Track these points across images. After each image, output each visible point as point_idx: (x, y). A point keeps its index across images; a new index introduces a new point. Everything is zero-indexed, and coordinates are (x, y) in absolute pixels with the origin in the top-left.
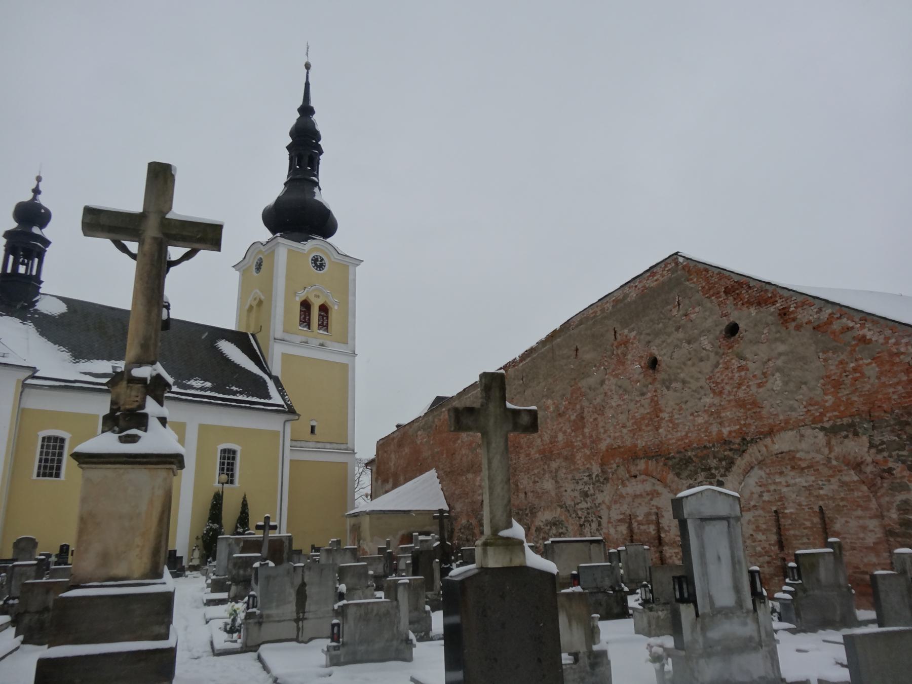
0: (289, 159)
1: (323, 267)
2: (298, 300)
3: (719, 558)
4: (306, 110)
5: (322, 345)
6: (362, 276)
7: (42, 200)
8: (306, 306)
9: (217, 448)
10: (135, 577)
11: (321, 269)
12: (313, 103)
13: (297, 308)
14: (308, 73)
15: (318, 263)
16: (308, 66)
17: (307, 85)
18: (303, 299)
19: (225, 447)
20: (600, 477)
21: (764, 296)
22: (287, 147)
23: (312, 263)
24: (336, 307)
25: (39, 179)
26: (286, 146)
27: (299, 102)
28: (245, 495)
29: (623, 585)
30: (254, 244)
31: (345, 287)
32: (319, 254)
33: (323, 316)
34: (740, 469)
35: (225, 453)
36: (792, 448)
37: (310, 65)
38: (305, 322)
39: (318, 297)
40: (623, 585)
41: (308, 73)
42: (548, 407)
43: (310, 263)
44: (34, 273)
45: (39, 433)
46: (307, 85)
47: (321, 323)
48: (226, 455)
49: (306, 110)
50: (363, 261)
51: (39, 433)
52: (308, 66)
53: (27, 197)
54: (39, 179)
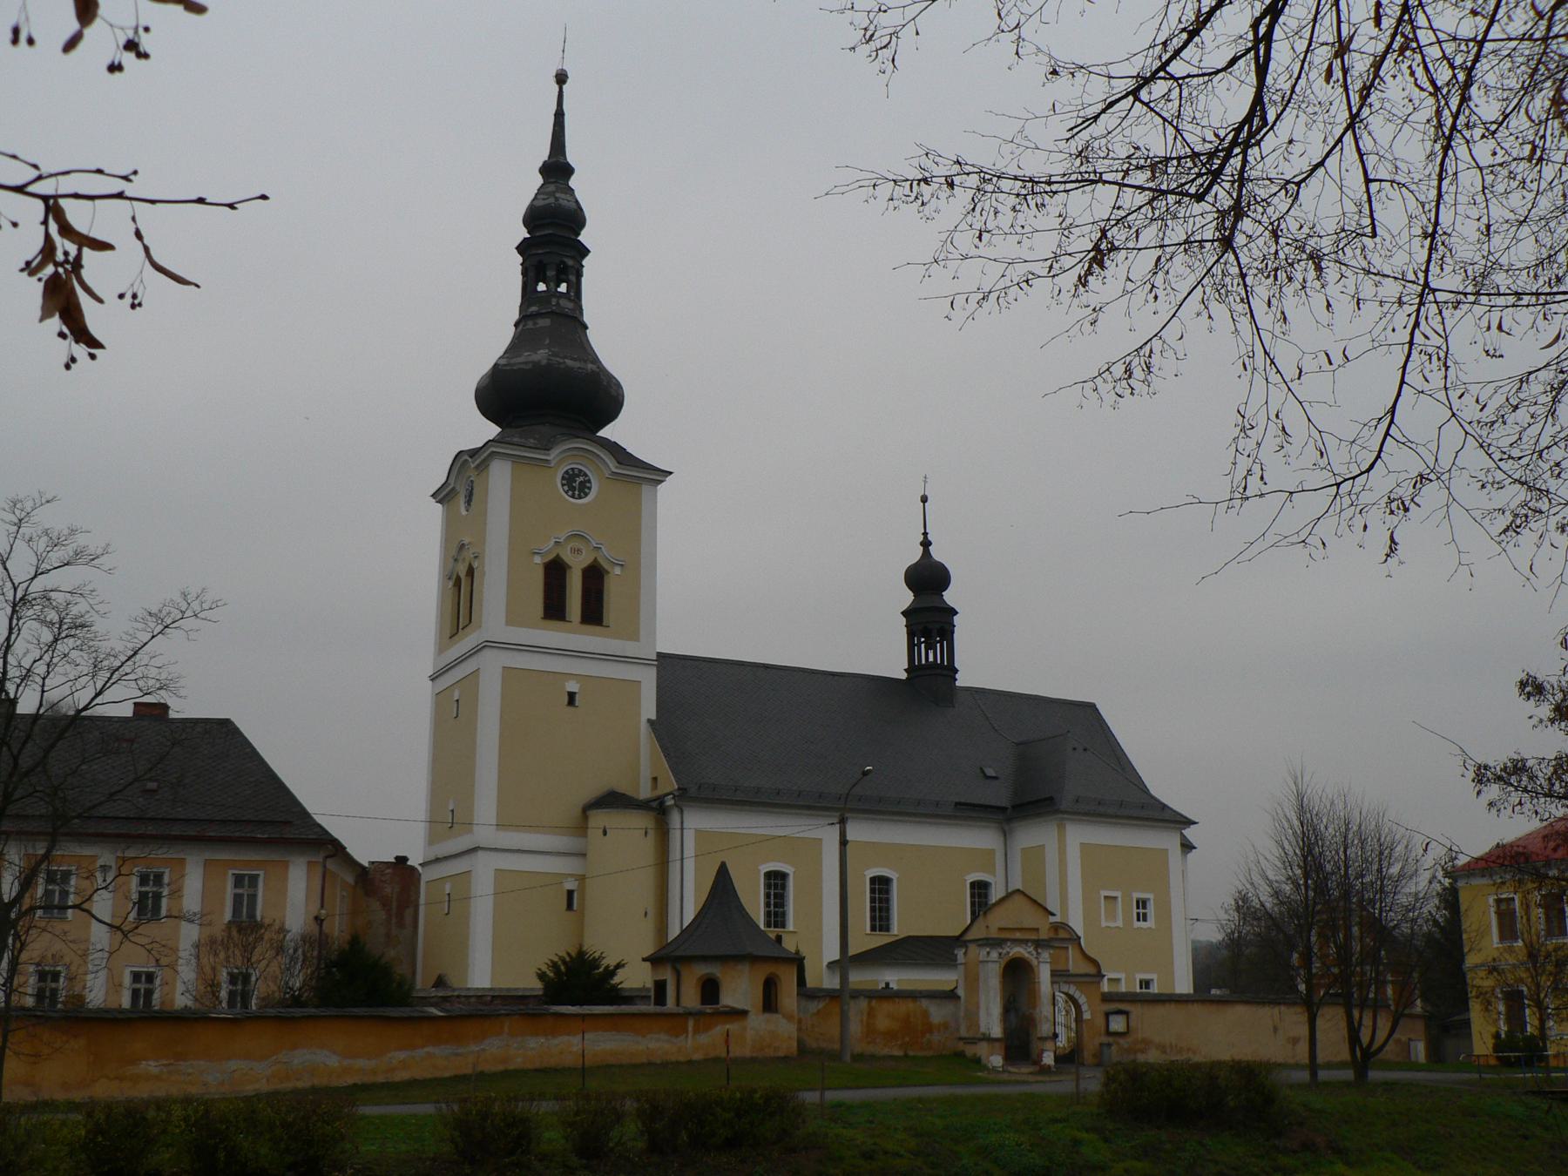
0: (522, 274)
1: (587, 490)
4: (557, 170)
8: (555, 572)
9: (759, 871)
11: (567, 476)
12: (572, 157)
16: (561, 78)
17: (559, 116)
19: (976, 879)
20: (153, 662)
22: (517, 248)
23: (563, 485)
26: (516, 244)
27: (543, 153)
28: (1195, 823)
30: (456, 456)
35: (770, 879)
36: (108, 864)
37: (567, 76)
39: (579, 551)
43: (559, 485)
45: (761, 868)
46: (559, 116)
48: (772, 881)
49: (557, 170)
50: (671, 473)
51: (761, 868)
52: (561, 78)
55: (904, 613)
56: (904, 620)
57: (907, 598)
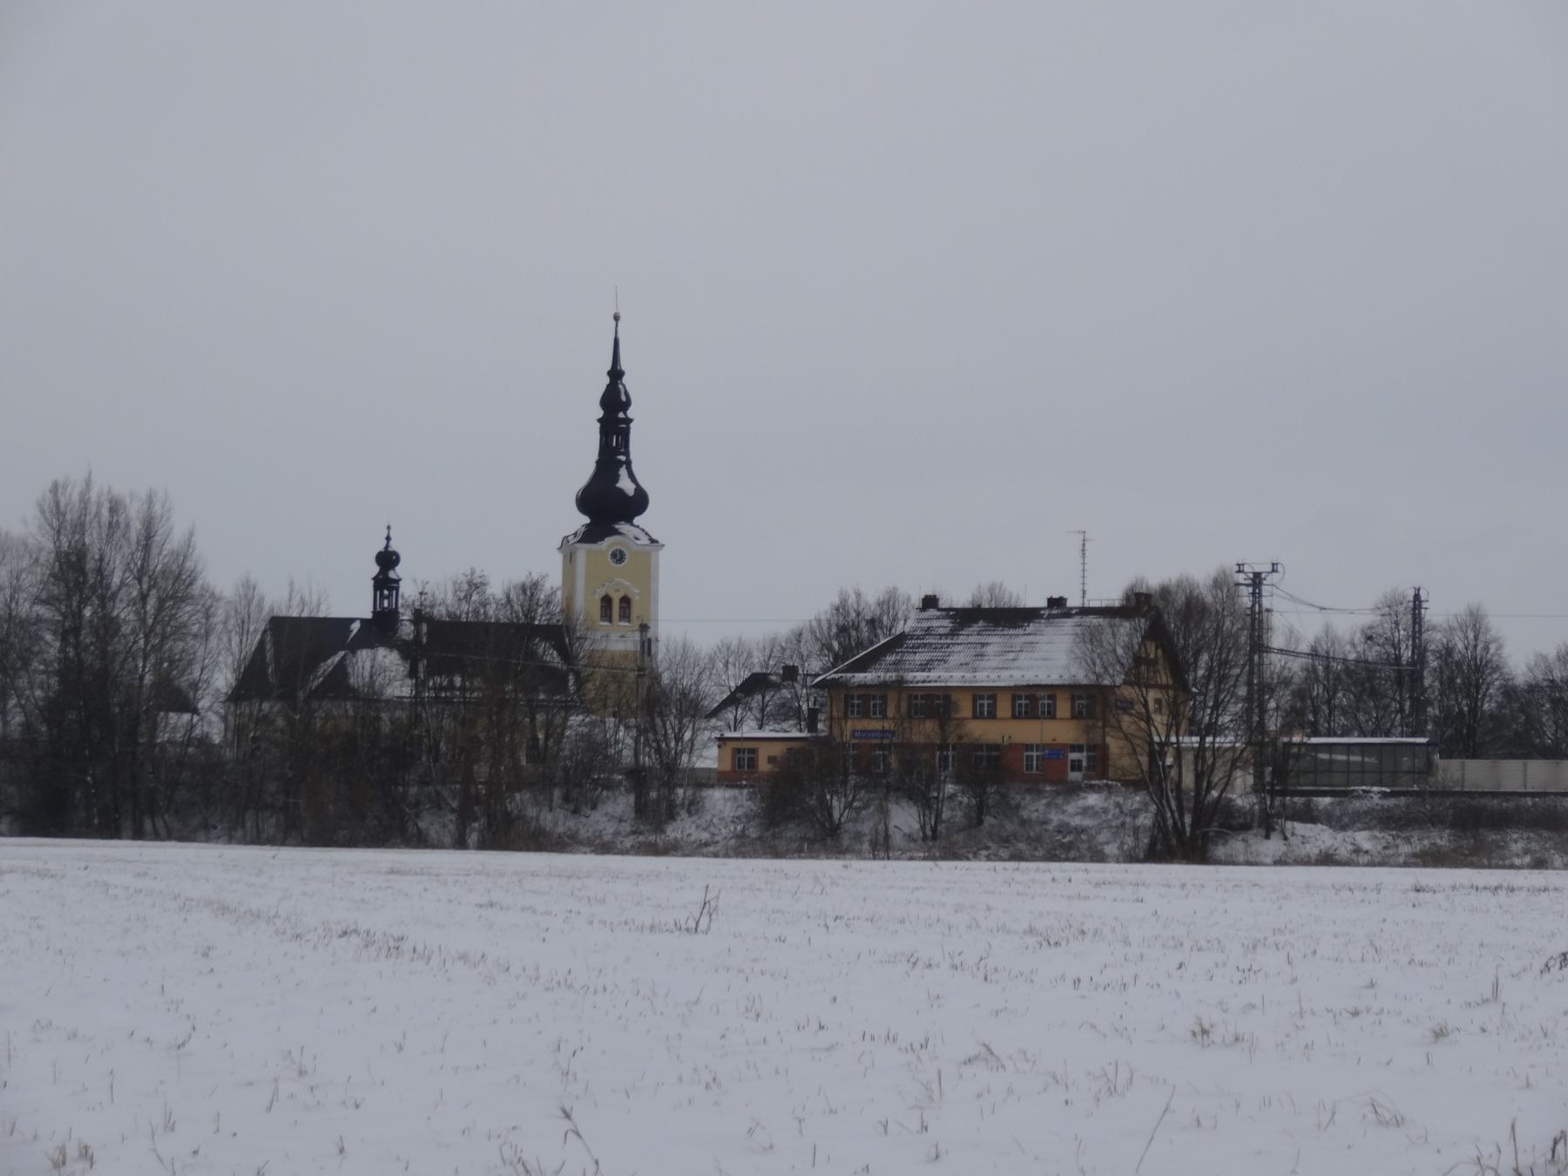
2: (598, 597)
3: (638, 993)
4: (616, 374)
5: (622, 637)
6: (666, 562)
7: (394, 546)
10: (943, 607)
13: (598, 605)
14: (617, 325)
15: (618, 557)
16: (616, 318)
18: (604, 595)
21: (791, 726)
24: (637, 598)
25: (389, 528)
27: (609, 367)
29: (1466, 671)
31: (647, 576)
32: (619, 547)
33: (625, 608)
34: (295, 1063)
38: (606, 616)
40: (1466, 671)
41: (617, 325)
42: (576, 811)
44: (394, 606)
47: (622, 614)
49: (616, 374)
52: (616, 318)
53: (381, 547)
54: (389, 528)
55: (599, 420)
56: (598, 425)
57: (607, 380)
